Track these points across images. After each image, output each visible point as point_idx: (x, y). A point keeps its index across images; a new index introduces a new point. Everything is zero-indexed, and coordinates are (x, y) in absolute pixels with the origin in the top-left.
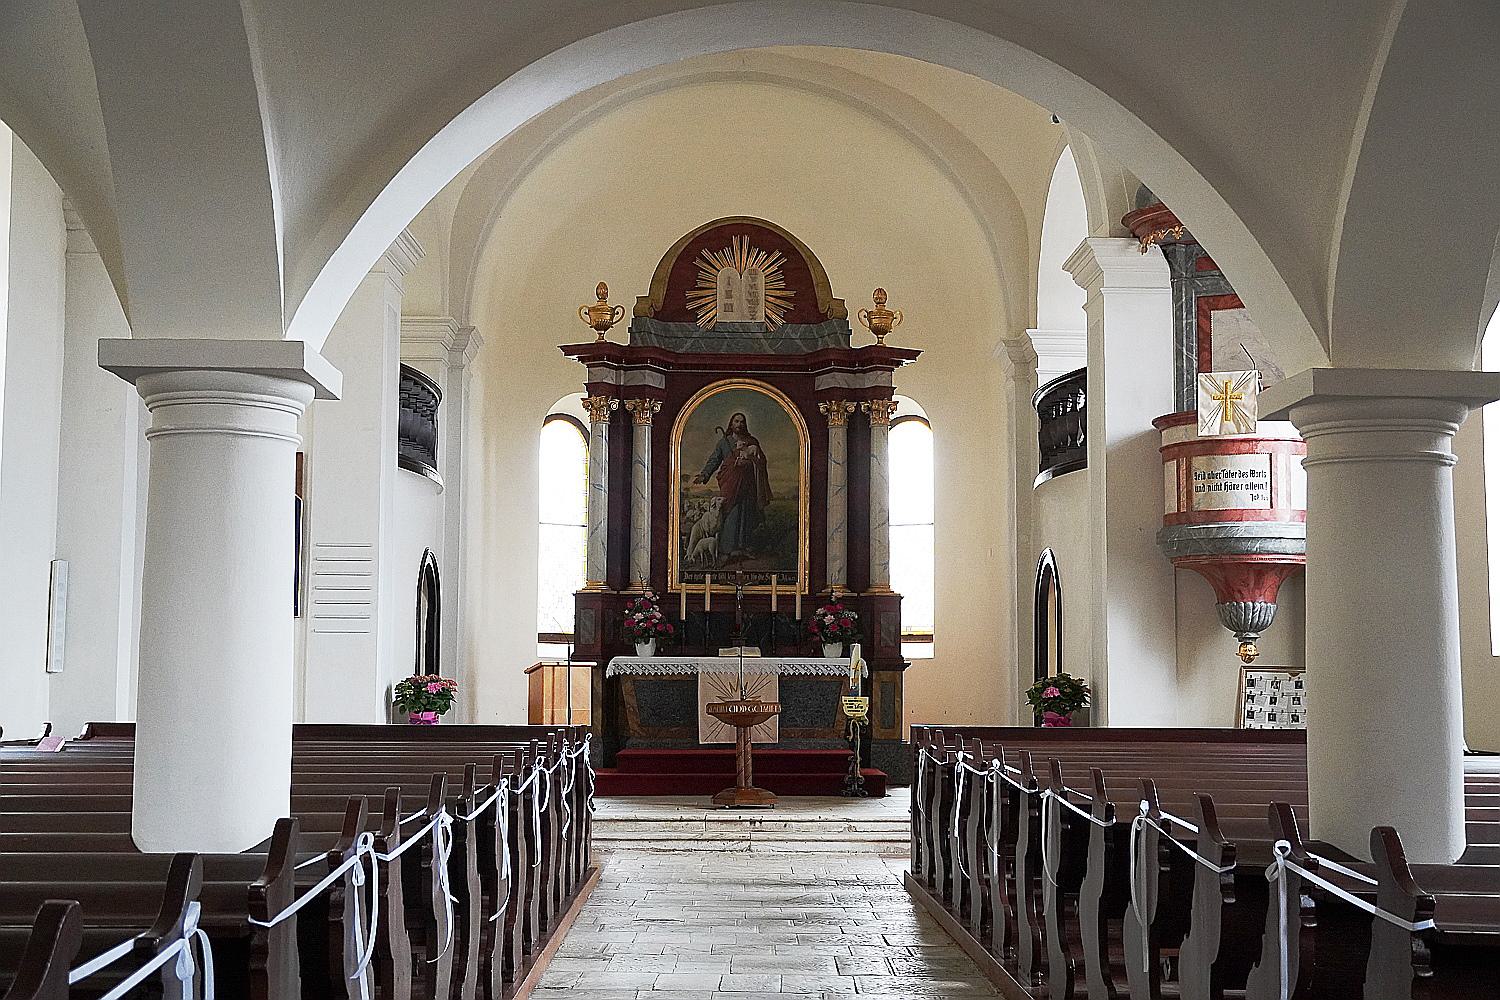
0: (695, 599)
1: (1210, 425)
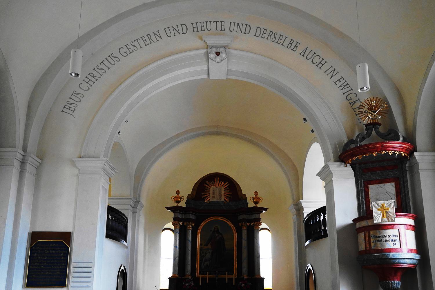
0: (204, 279)
1: (378, 219)
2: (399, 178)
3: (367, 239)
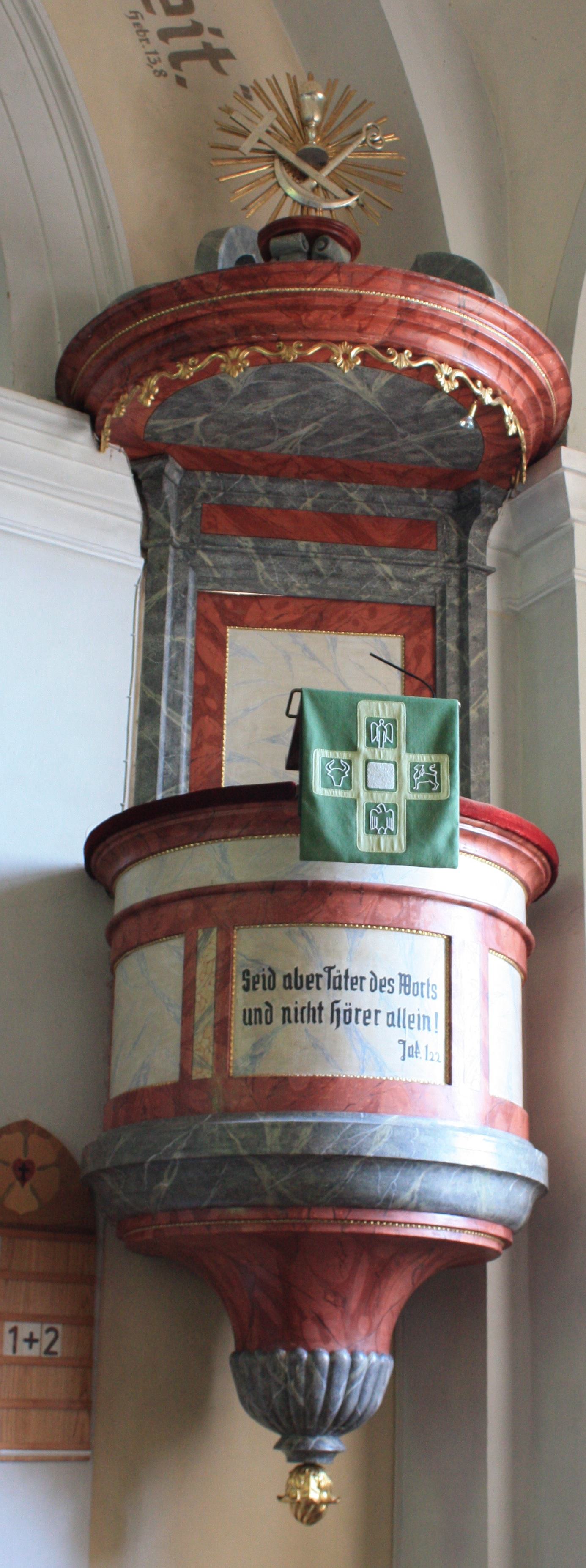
2: (433, 609)
3: (205, 992)
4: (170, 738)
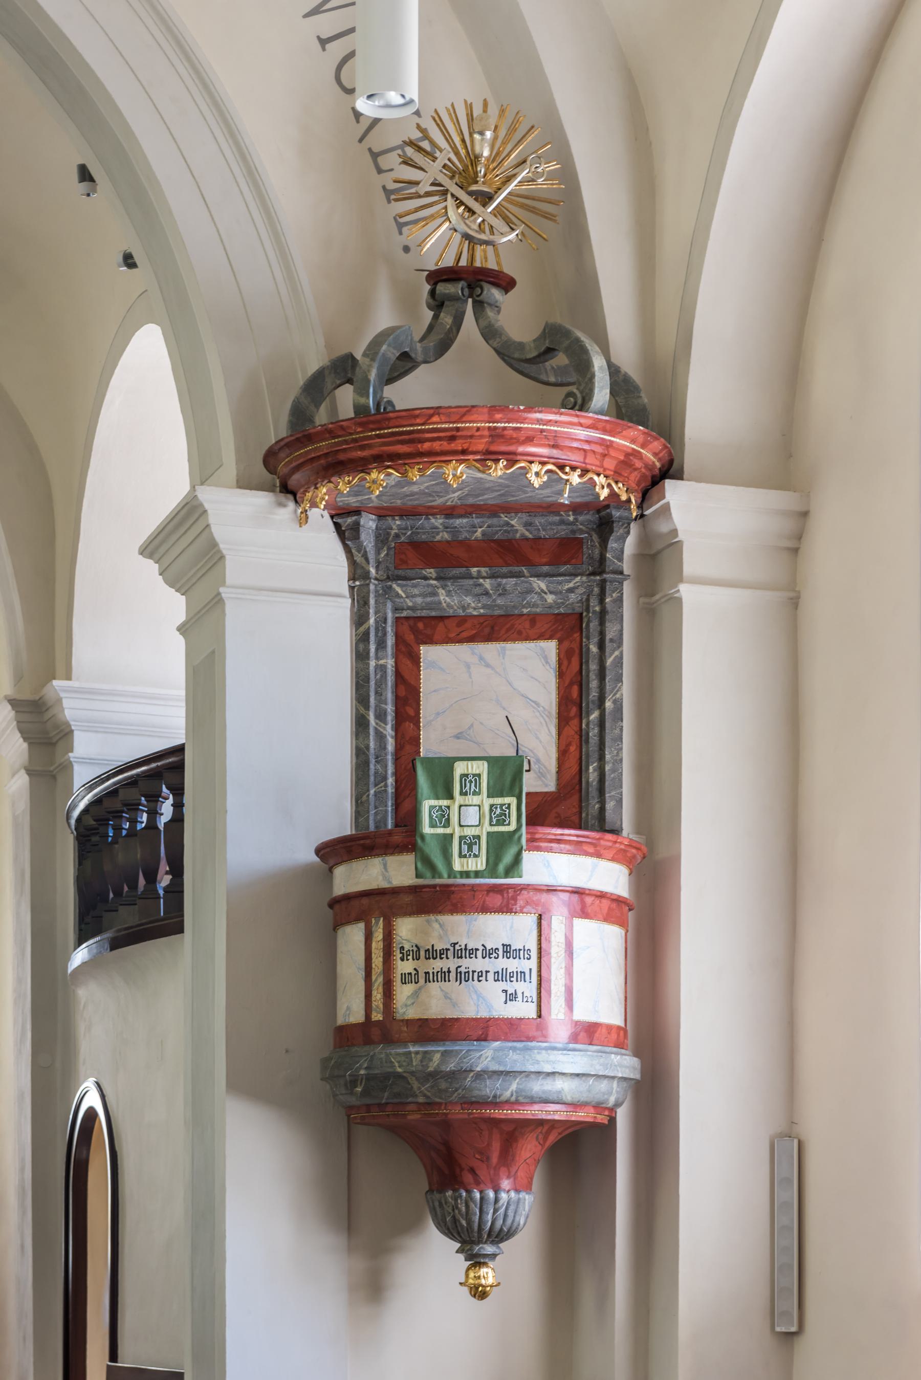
2: (581, 614)
4: (378, 744)
